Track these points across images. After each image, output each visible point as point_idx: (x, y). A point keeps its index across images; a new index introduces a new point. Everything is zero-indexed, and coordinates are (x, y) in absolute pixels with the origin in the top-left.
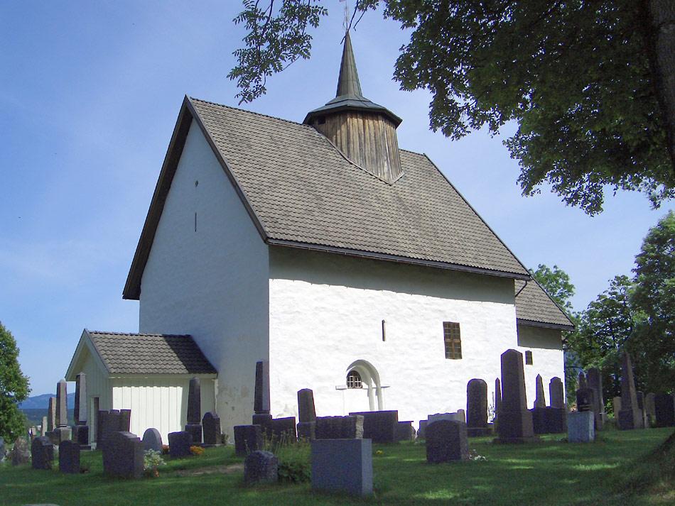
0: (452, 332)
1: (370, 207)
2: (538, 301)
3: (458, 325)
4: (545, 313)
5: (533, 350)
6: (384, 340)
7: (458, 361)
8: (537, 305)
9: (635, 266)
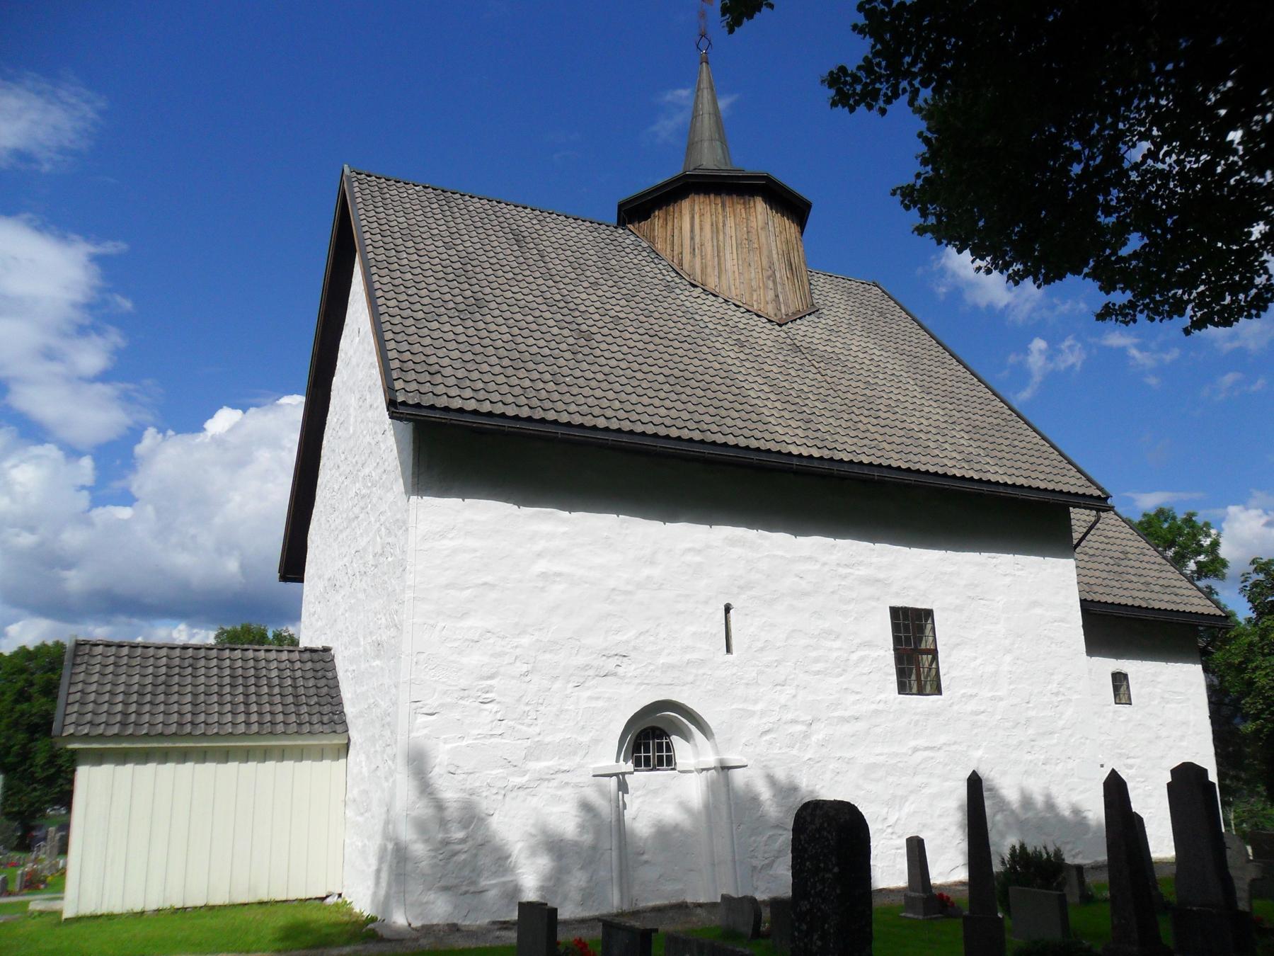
0: (912, 637)
1: (909, 442)
2: (1137, 564)
3: (929, 614)
4: (1160, 586)
5: (1130, 666)
6: (729, 650)
7: (661, 775)
8: (1132, 571)
9: (1030, 849)
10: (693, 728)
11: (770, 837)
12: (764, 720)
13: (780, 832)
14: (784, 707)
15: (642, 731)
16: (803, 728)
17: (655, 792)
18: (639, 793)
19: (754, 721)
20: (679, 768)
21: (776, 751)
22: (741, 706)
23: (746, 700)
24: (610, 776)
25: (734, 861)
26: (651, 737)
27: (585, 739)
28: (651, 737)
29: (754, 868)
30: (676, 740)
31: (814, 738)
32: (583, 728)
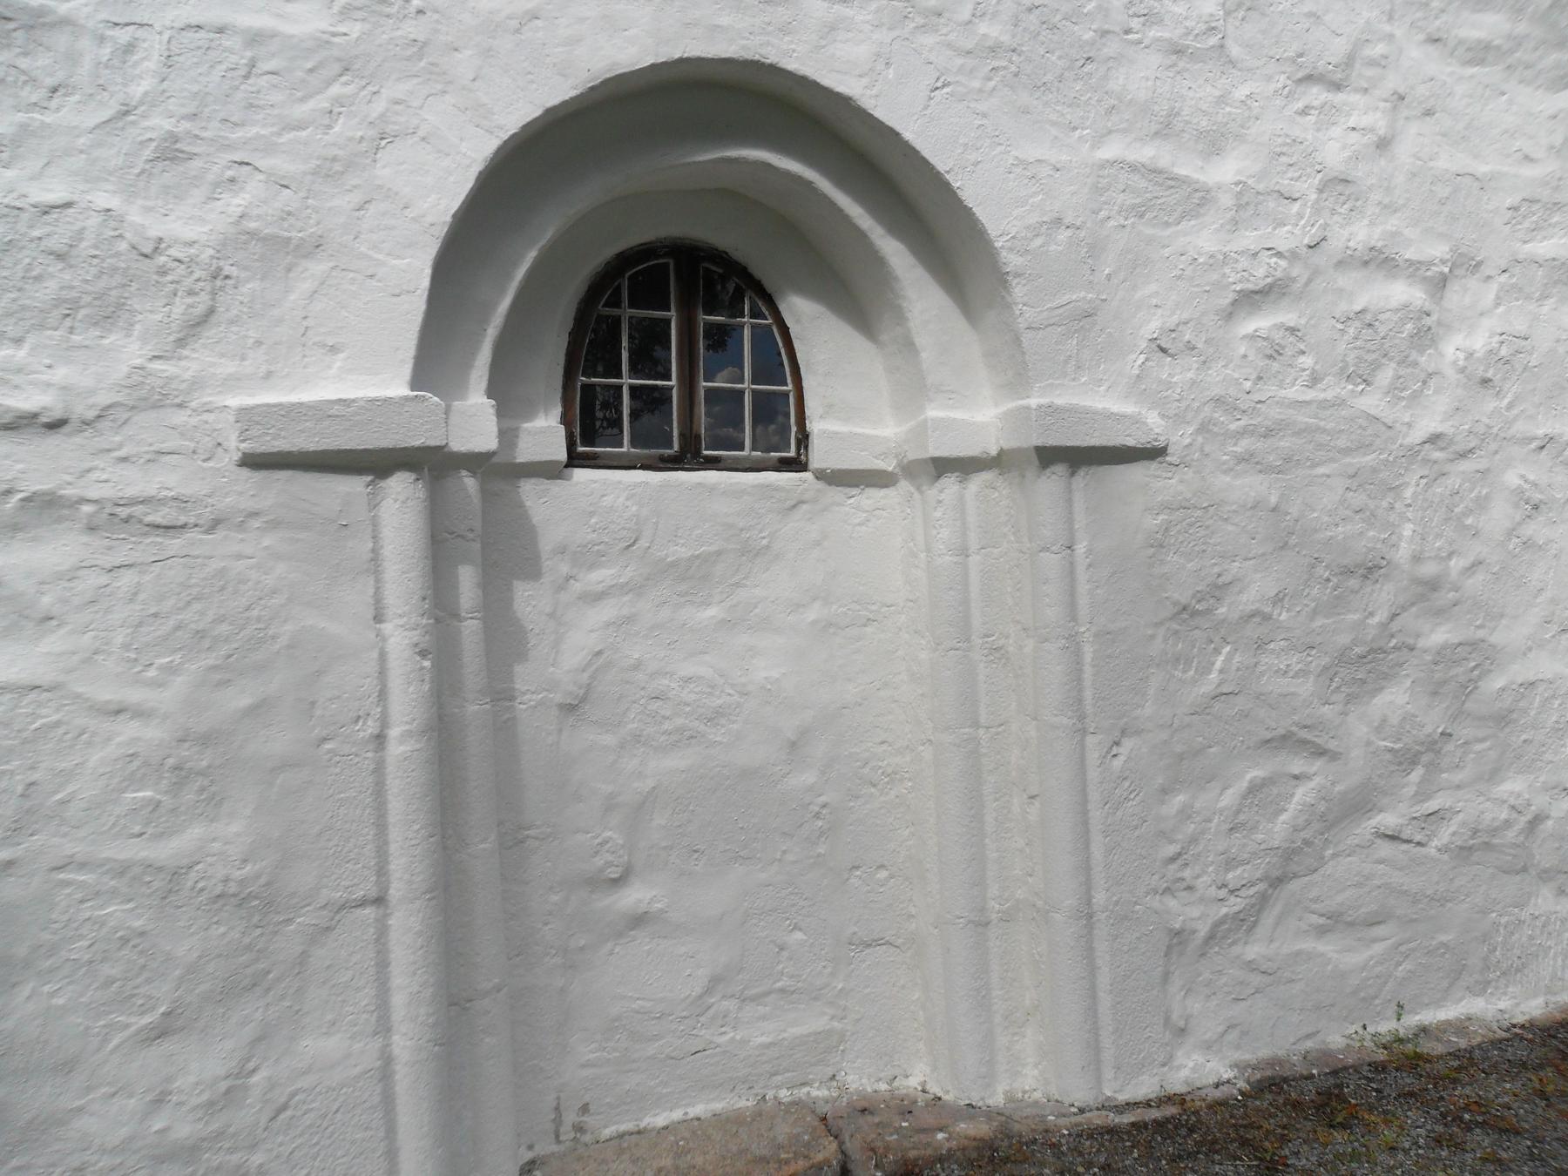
10: (894, 251)
11: (1254, 789)
12: (1249, 239)
13: (1297, 766)
14: (1337, 184)
15: (645, 252)
16: (1417, 295)
17: (693, 576)
18: (600, 576)
19: (1204, 238)
20: (819, 456)
21: (1294, 392)
22: (1145, 153)
23: (1166, 130)
24: (376, 464)
25: (1087, 915)
26: (667, 278)
27: (189, 224)
28: (667, 278)
29: (1178, 937)
30: (804, 315)
31: (1452, 348)
32: (170, 152)
